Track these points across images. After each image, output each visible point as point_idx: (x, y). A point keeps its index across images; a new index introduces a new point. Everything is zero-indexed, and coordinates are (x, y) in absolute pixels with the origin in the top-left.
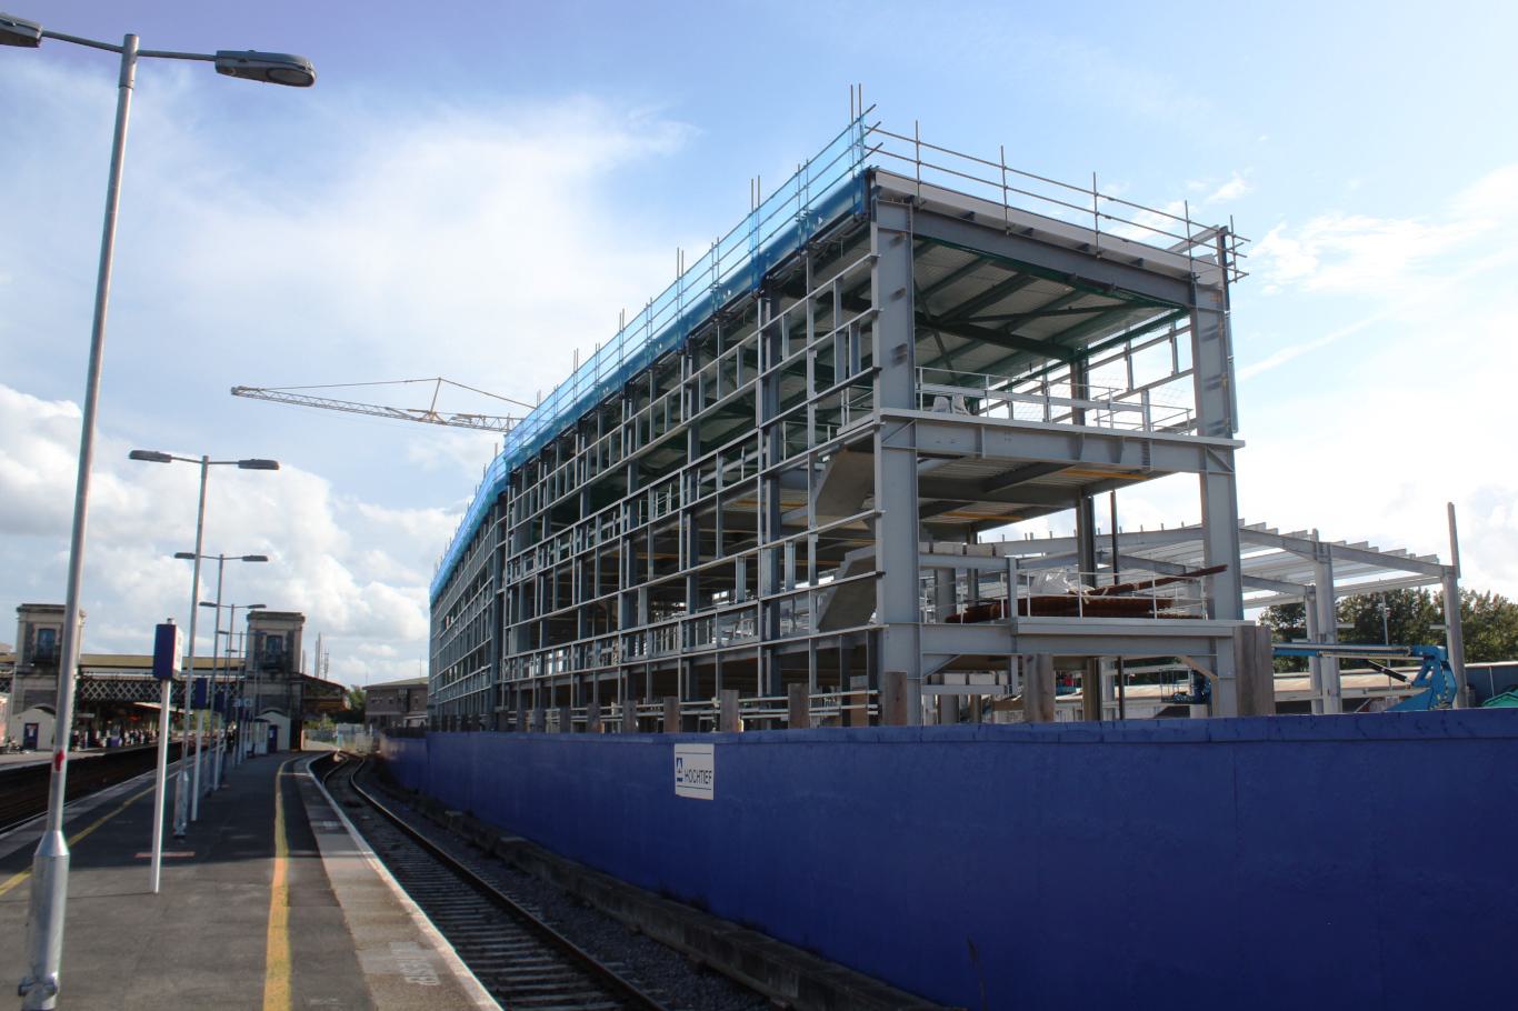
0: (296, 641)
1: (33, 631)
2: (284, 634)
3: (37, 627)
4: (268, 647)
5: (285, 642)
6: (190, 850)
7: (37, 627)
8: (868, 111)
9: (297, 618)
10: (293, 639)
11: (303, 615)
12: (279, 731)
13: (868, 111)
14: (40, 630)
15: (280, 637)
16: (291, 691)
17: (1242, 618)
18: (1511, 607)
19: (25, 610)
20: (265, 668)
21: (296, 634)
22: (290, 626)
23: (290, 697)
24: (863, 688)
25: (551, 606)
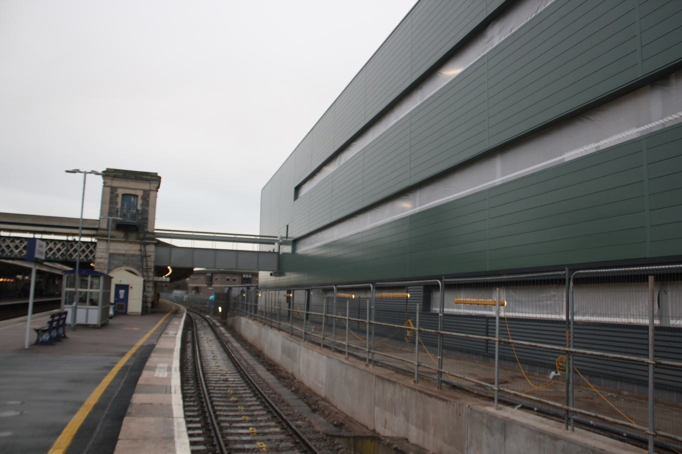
0: (151, 202)
1: (117, 196)
2: (140, 193)
3: (120, 192)
4: (123, 205)
5: (140, 202)
6: (346, 302)
7: (120, 192)
8: (414, 131)
9: (153, 179)
10: (148, 199)
11: (159, 175)
12: (131, 292)
13: (414, 131)
14: (124, 195)
15: (136, 196)
16: (145, 251)
17: (65, 303)
18: (656, 319)
19: (109, 174)
20: (120, 227)
21: (152, 194)
22: (146, 186)
23: (144, 256)
24: (498, 376)
25: (364, 322)
